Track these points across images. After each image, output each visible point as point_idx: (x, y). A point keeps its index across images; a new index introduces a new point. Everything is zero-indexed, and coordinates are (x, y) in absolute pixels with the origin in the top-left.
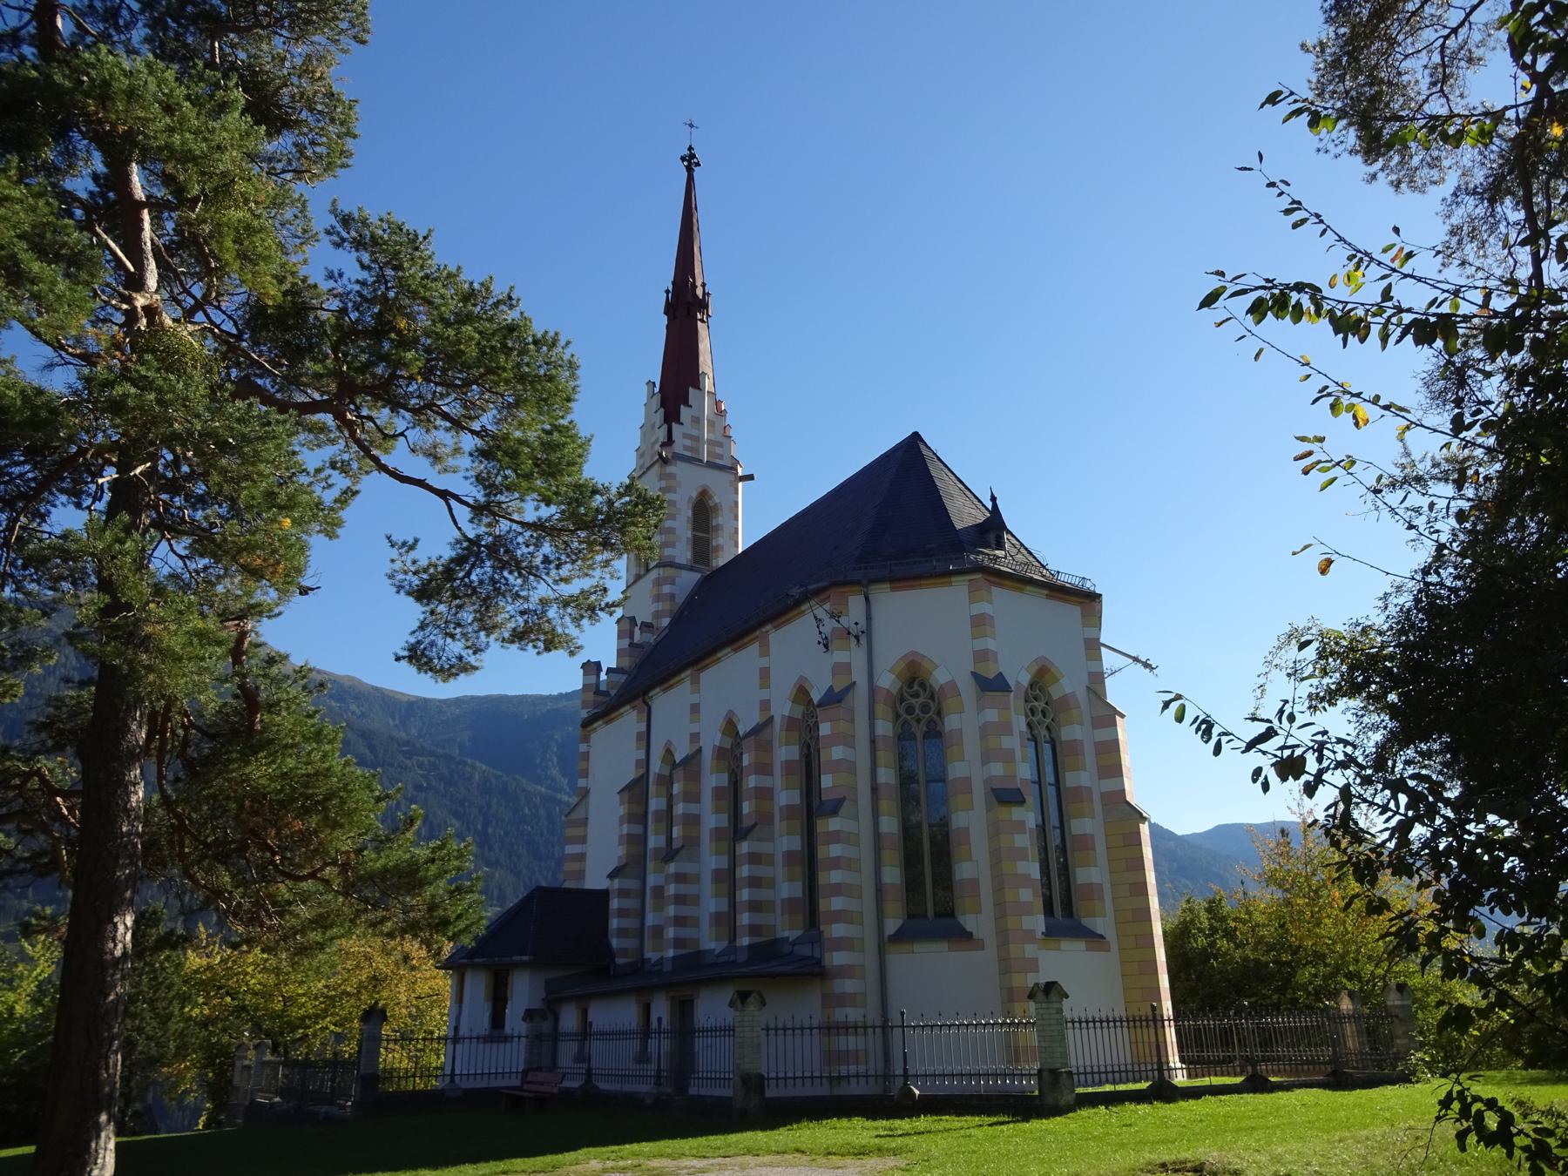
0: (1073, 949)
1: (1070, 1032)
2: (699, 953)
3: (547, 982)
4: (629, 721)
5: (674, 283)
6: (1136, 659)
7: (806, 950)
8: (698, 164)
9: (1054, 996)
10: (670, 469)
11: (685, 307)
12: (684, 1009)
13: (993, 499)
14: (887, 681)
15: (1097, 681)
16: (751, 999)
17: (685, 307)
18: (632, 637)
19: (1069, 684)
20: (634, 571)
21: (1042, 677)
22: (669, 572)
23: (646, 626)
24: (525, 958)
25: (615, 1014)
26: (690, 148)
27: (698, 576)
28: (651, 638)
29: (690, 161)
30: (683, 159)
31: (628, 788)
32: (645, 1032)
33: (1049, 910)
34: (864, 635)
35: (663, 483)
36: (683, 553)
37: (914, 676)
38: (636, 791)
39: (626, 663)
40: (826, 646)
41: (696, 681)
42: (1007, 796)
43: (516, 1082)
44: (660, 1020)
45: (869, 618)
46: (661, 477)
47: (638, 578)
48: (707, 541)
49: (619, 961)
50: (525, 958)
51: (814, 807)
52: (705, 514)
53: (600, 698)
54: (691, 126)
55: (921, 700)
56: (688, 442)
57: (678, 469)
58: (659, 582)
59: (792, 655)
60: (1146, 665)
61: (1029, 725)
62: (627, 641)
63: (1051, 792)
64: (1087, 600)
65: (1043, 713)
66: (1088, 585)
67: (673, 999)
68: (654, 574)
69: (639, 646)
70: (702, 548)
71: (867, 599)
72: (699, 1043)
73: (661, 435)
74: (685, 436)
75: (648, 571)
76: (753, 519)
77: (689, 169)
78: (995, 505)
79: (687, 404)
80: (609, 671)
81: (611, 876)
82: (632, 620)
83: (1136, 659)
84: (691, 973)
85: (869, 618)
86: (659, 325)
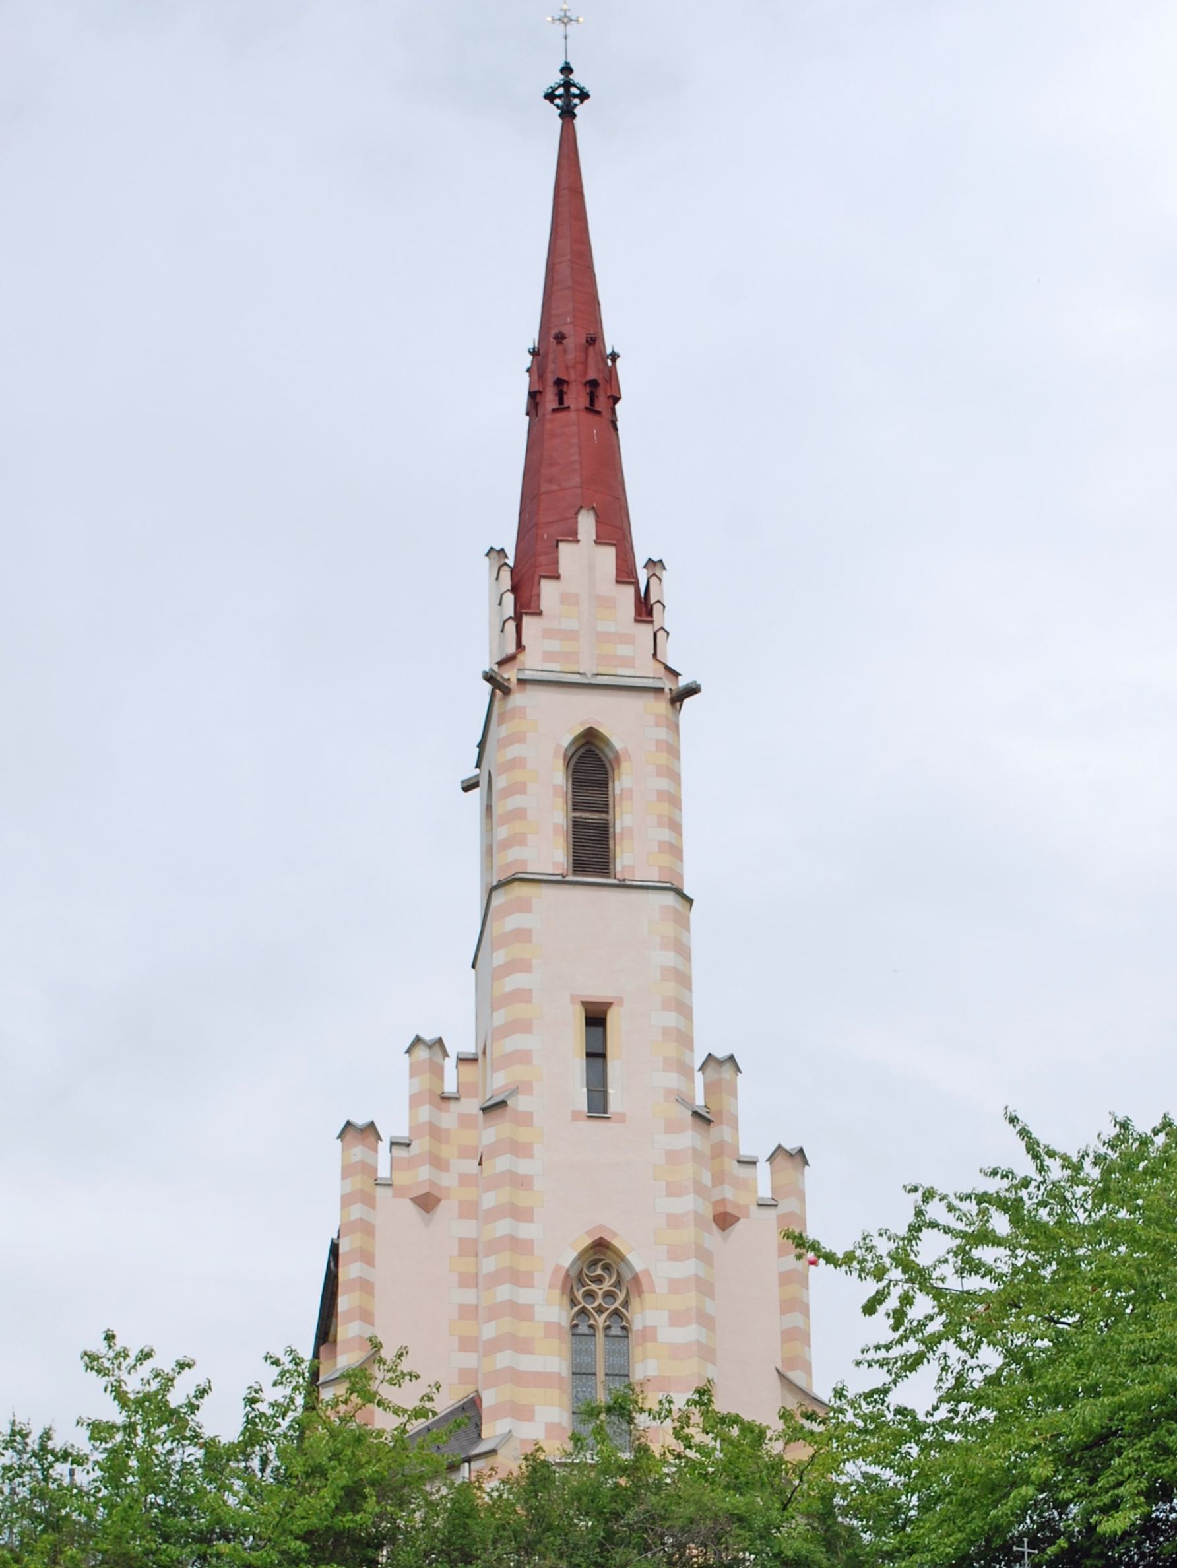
11: (573, 383)
17: (573, 383)
26: (567, 70)
29: (567, 97)
55: (606, 1286)
56: (555, 645)
74: (548, 634)
77: (568, 114)
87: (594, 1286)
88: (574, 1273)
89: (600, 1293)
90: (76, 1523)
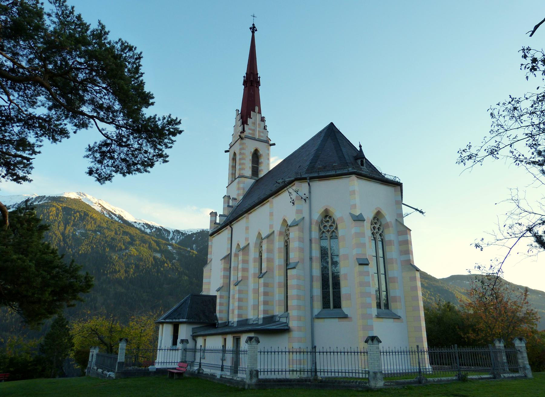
0: (389, 323)
1: (382, 356)
2: (247, 320)
3: (193, 329)
4: (225, 233)
5: (247, 74)
6: (417, 210)
7: (284, 320)
8: (256, 30)
9: (375, 342)
10: (244, 141)
11: (252, 82)
12: (237, 341)
13: (360, 146)
14: (317, 216)
15: (400, 216)
16: (253, 340)
17: (252, 82)
18: (229, 203)
19: (389, 217)
20: (230, 180)
21: (378, 216)
22: (243, 179)
23: (235, 199)
24: (184, 320)
25: (214, 342)
26: (253, 25)
27: (254, 181)
28: (236, 204)
29: (253, 29)
30: (251, 28)
31: (224, 258)
32: (224, 350)
33: (379, 306)
34: (307, 199)
35: (241, 146)
36: (248, 172)
37: (327, 215)
38: (228, 258)
39: (226, 213)
40: (293, 203)
41: (248, 218)
42: (364, 263)
43: (176, 366)
44: (201, 346)
45: (310, 192)
46: (241, 144)
47: (232, 182)
48: (257, 168)
49: (220, 322)
50: (184, 320)
51: (287, 266)
52: (256, 157)
53: (217, 225)
54: (254, 16)
55: (330, 224)
56: (250, 132)
57: (246, 141)
58: (239, 183)
59: (282, 208)
60: (421, 212)
61: (373, 234)
62: (227, 205)
63: (381, 260)
64: (397, 185)
65: (379, 229)
66: (397, 180)
67: (234, 337)
68: (237, 180)
69: (232, 207)
70: (255, 171)
71: (309, 184)
72: (241, 356)
73: (240, 129)
74: (250, 129)
75: (235, 179)
76: (274, 160)
77: (253, 32)
78: (361, 149)
79: (250, 118)
80: (220, 216)
81: (217, 291)
82: (229, 197)
83: (417, 210)
84: (244, 328)
85: (310, 192)
86: (241, 88)
87: (326, 224)
88: (320, 221)
89: (328, 226)
90: (124, 71)
